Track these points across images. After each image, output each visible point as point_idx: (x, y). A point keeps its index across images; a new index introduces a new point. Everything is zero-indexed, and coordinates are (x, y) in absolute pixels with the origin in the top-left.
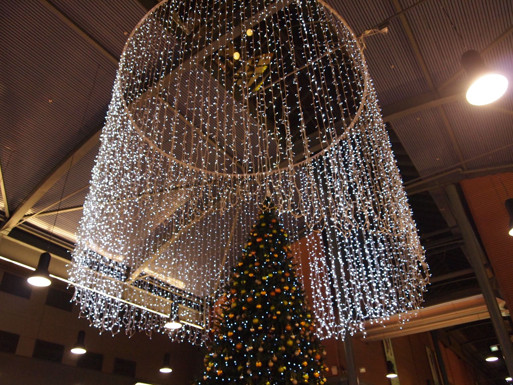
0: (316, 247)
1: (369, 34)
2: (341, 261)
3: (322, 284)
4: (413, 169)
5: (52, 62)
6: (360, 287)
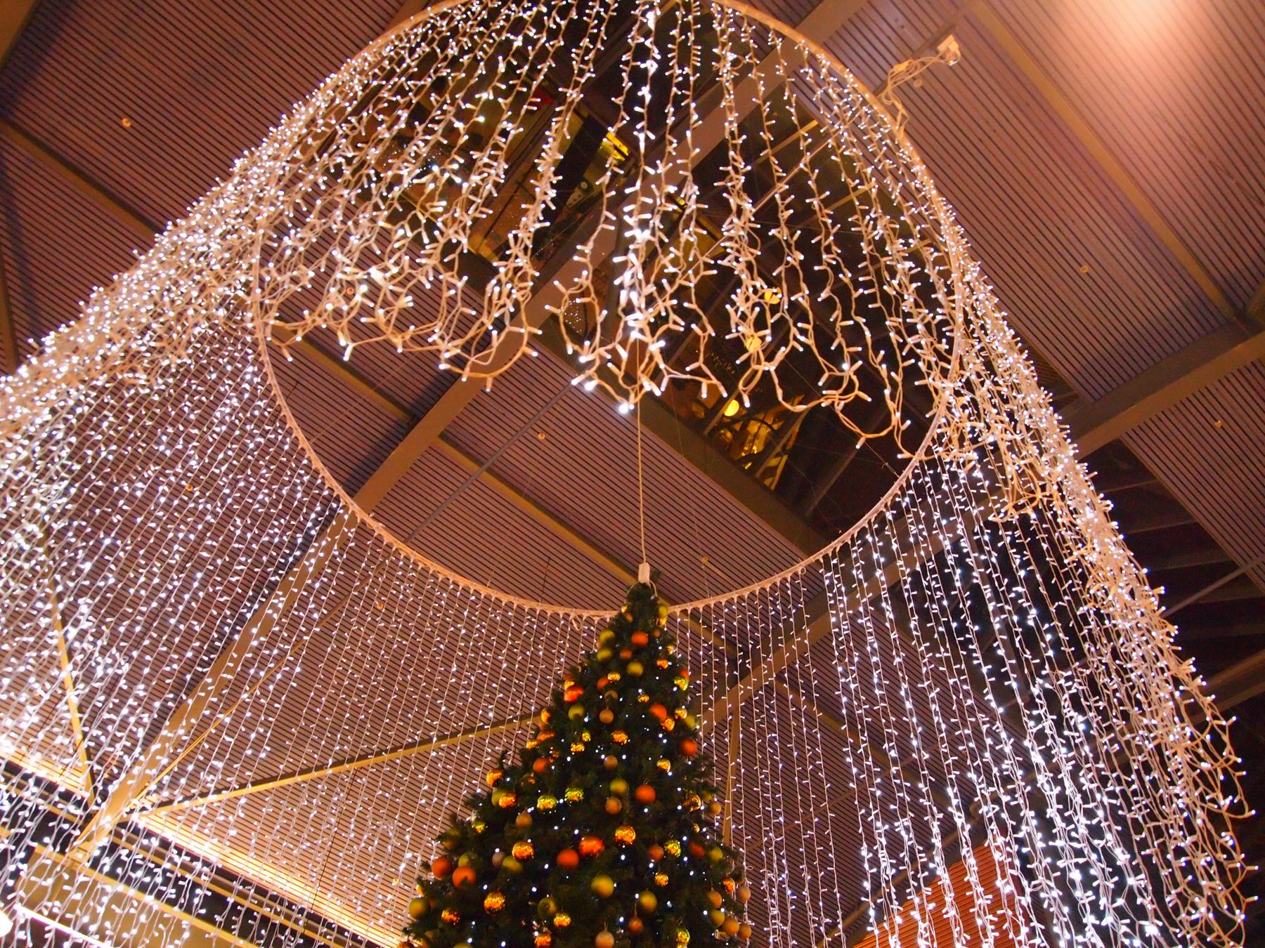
0: (878, 786)
1: (908, 71)
2: (959, 819)
3: (905, 915)
4: (1197, 537)
5: (117, 250)
6: (1029, 899)
